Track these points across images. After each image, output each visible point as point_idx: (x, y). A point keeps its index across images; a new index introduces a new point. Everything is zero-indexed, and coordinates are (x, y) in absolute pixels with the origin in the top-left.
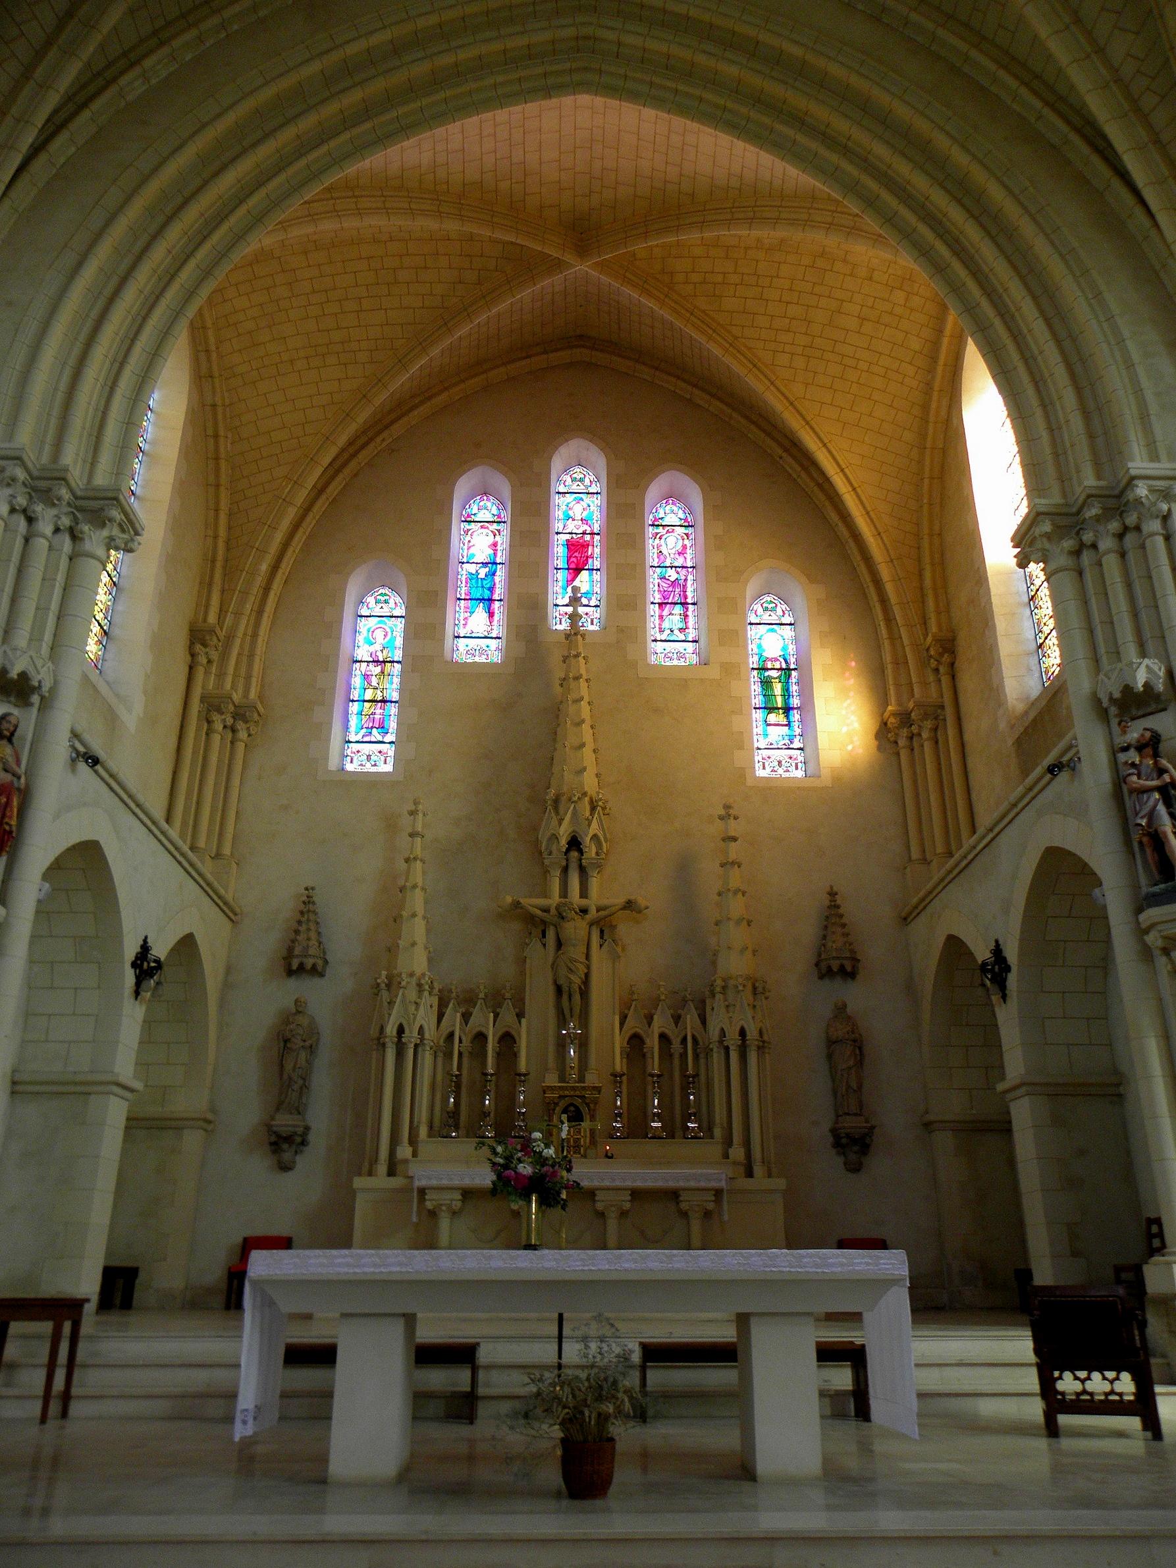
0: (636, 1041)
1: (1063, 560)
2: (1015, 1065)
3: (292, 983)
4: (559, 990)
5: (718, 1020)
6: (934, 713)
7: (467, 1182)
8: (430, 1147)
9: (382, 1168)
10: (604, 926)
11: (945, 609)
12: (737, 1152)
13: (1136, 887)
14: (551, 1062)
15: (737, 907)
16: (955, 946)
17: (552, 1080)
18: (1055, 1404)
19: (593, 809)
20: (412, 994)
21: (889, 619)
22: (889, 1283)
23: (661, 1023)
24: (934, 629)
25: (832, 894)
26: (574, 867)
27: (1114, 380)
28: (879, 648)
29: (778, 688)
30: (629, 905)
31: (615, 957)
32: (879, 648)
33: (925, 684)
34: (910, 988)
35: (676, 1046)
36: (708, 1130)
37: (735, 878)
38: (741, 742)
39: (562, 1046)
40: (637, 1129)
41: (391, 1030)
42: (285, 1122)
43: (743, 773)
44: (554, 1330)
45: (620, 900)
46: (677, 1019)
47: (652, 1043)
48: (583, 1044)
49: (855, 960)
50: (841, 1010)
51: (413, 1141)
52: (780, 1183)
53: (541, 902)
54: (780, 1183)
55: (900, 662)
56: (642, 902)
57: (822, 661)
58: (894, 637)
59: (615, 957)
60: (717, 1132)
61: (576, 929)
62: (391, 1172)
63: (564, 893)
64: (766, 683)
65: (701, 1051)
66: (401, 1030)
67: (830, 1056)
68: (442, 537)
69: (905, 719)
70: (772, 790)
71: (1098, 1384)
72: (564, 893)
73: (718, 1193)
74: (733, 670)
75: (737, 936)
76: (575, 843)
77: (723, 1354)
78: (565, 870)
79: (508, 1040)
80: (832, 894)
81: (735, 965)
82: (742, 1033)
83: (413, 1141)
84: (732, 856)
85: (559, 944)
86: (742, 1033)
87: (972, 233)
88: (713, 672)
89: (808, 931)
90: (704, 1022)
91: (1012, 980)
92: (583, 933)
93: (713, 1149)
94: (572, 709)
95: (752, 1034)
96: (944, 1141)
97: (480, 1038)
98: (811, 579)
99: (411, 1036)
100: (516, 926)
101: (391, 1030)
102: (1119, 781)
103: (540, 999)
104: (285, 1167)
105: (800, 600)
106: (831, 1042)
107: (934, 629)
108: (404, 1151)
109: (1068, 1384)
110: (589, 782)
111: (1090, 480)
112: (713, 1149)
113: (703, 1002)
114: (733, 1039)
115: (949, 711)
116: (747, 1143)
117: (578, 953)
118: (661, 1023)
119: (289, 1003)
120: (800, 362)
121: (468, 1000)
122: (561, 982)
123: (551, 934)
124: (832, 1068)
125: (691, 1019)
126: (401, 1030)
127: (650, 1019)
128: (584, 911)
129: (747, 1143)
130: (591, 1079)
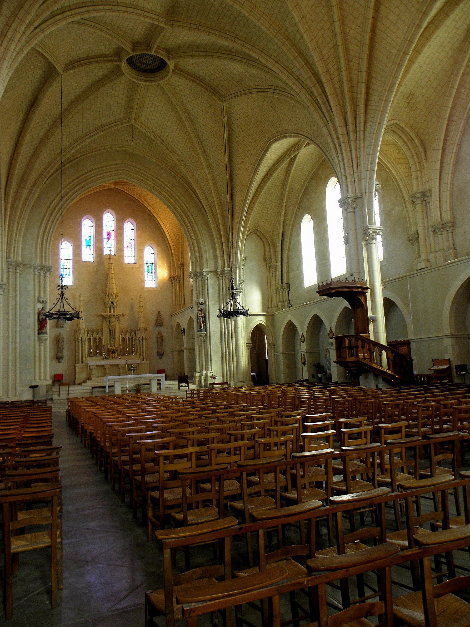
0: (123, 339)
1: (194, 280)
2: (185, 346)
3: (57, 329)
4: (110, 330)
5: (138, 335)
6: (179, 278)
7: (97, 364)
8: (88, 358)
9: (80, 362)
10: (118, 318)
11: (183, 257)
12: (141, 357)
13: (198, 328)
14: (109, 343)
15: (142, 315)
16: (178, 324)
17: (109, 346)
18: (179, 387)
19: (116, 296)
20: (83, 332)
21: (172, 256)
22: (163, 376)
23: (128, 335)
24: (180, 261)
25: (159, 311)
26: (112, 307)
27: (204, 254)
28: (170, 262)
29: (150, 267)
30: (122, 314)
31: (119, 323)
32: (170, 262)
33: (178, 271)
34: (172, 328)
35: (131, 339)
36: (136, 353)
37: (142, 310)
38: (143, 281)
39: (111, 340)
40: (124, 354)
41: (80, 338)
42: (160, 352)
43: (143, 287)
44: (70, 392)
45: (121, 313)
46: (131, 334)
47: (126, 339)
48: (114, 339)
49: (162, 324)
50: (159, 333)
51: (85, 357)
52: (148, 362)
53: (106, 314)
54: (148, 362)
55: (174, 266)
56: (125, 314)
57: (159, 263)
58: (173, 260)
59: (119, 323)
60: (138, 354)
61: (113, 319)
62: (82, 363)
63: (110, 312)
64: (148, 266)
65: (136, 340)
66: (82, 338)
67: (157, 340)
68: (80, 231)
69: (174, 278)
70: (150, 290)
71: (183, 385)
72: (110, 312)
73: (139, 364)
74: (142, 266)
75: (142, 320)
76: (112, 303)
77: (148, 384)
78: (110, 308)
79: (100, 339)
80: (159, 311)
81: (141, 325)
82: (143, 337)
83: (85, 357)
84: (141, 305)
85: (110, 322)
86: (143, 337)
87: (187, 221)
88: (137, 266)
89: (154, 318)
90: (135, 335)
91: (185, 333)
92: (114, 320)
93: (137, 357)
94: (111, 275)
95: (144, 338)
96: (176, 354)
97: (95, 339)
98: (158, 245)
99: (84, 339)
100: (100, 317)
101: (80, 338)
102: (197, 315)
103: (106, 331)
104: (59, 362)
105: (155, 249)
106: (157, 338)
107: (180, 261)
108: (84, 359)
109: (181, 385)
110: (115, 291)
111: (199, 270)
112: (137, 357)
113: (135, 331)
114: (141, 339)
115: (182, 277)
116: (143, 356)
117: (113, 324)
118: (128, 335)
119: (58, 333)
120: (158, 204)
121: (93, 332)
122: (111, 328)
123: (108, 320)
124: (158, 343)
125: (133, 334)
126: (82, 338)
127: (126, 335)
128: (114, 315)
129: (143, 356)
130: (116, 346)
